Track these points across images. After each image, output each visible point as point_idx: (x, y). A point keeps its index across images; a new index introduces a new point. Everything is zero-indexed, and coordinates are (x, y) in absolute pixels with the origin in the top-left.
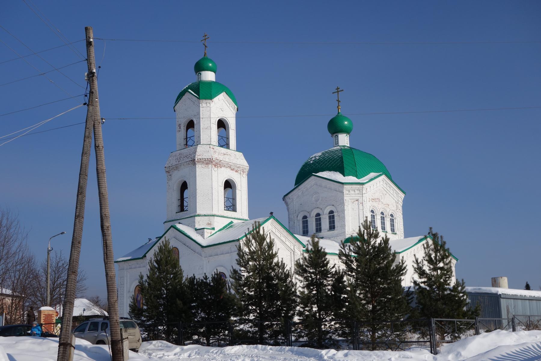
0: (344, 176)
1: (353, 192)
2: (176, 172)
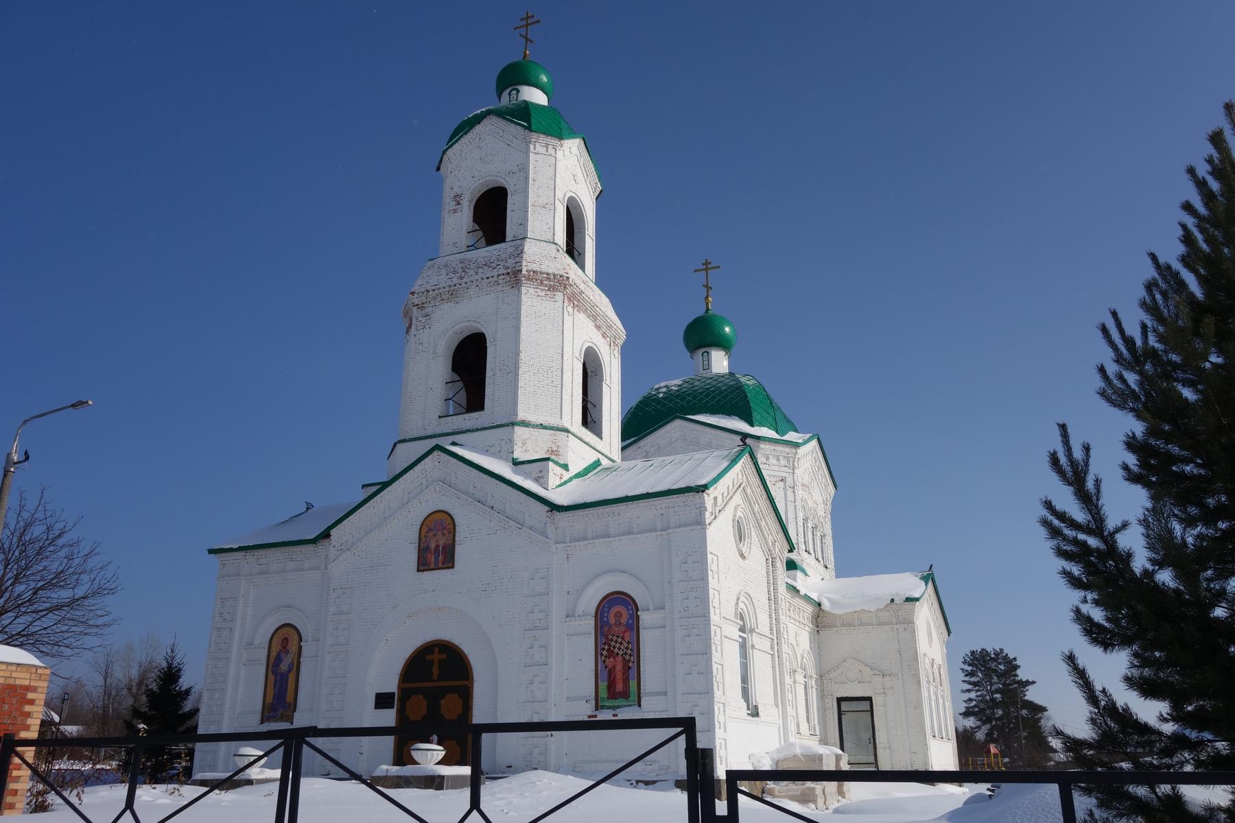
0: (752, 425)
1: (775, 461)
2: (446, 307)
